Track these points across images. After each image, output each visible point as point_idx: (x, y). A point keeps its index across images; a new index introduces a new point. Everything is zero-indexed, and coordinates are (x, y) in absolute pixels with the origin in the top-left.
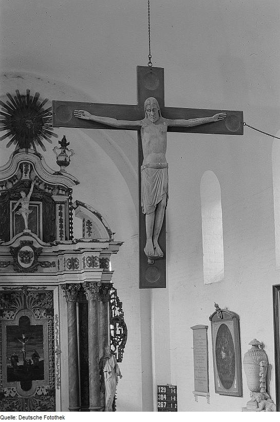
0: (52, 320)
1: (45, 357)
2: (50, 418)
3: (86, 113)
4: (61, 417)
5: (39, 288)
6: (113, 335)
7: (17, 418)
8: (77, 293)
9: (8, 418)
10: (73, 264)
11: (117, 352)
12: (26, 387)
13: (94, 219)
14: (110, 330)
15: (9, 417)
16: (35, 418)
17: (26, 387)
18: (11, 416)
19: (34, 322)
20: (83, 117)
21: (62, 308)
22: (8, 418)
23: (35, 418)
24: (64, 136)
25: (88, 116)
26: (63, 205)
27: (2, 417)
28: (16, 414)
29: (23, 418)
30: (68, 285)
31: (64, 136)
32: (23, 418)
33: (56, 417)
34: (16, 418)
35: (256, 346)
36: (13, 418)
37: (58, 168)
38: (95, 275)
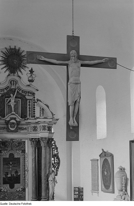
0: (25, 155)
1: (21, 173)
2: (24, 204)
3: (42, 57)
4: (29, 204)
5: (18, 140)
6: (53, 163)
7: (8, 204)
8: (37, 143)
9: (4, 204)
10: (35, 129)
11: (55, 171)
12: (12, 187)
13: (45, 107)
14: (52, 160)
15: (4, 204)
16: (17, 204)
17: (12, 187)
18: (6, 203)
19: (16, 156)
20: (41, 59)
21: (29, 149)
22: (4, 204)
23: (17, 204)
24: (32, 68)
25: (43, 58)
26: (31, 101)
27: (1, 204)
28: (7, 202)
29: (11, 204)
30: (32, 139)
31: (32, 68)
32: (11, 204)
33: (27, 204)
34: (8, 204)
35: (121, 169)
36: (6, 204)
37: (29, 83)
38: (45, 134)
